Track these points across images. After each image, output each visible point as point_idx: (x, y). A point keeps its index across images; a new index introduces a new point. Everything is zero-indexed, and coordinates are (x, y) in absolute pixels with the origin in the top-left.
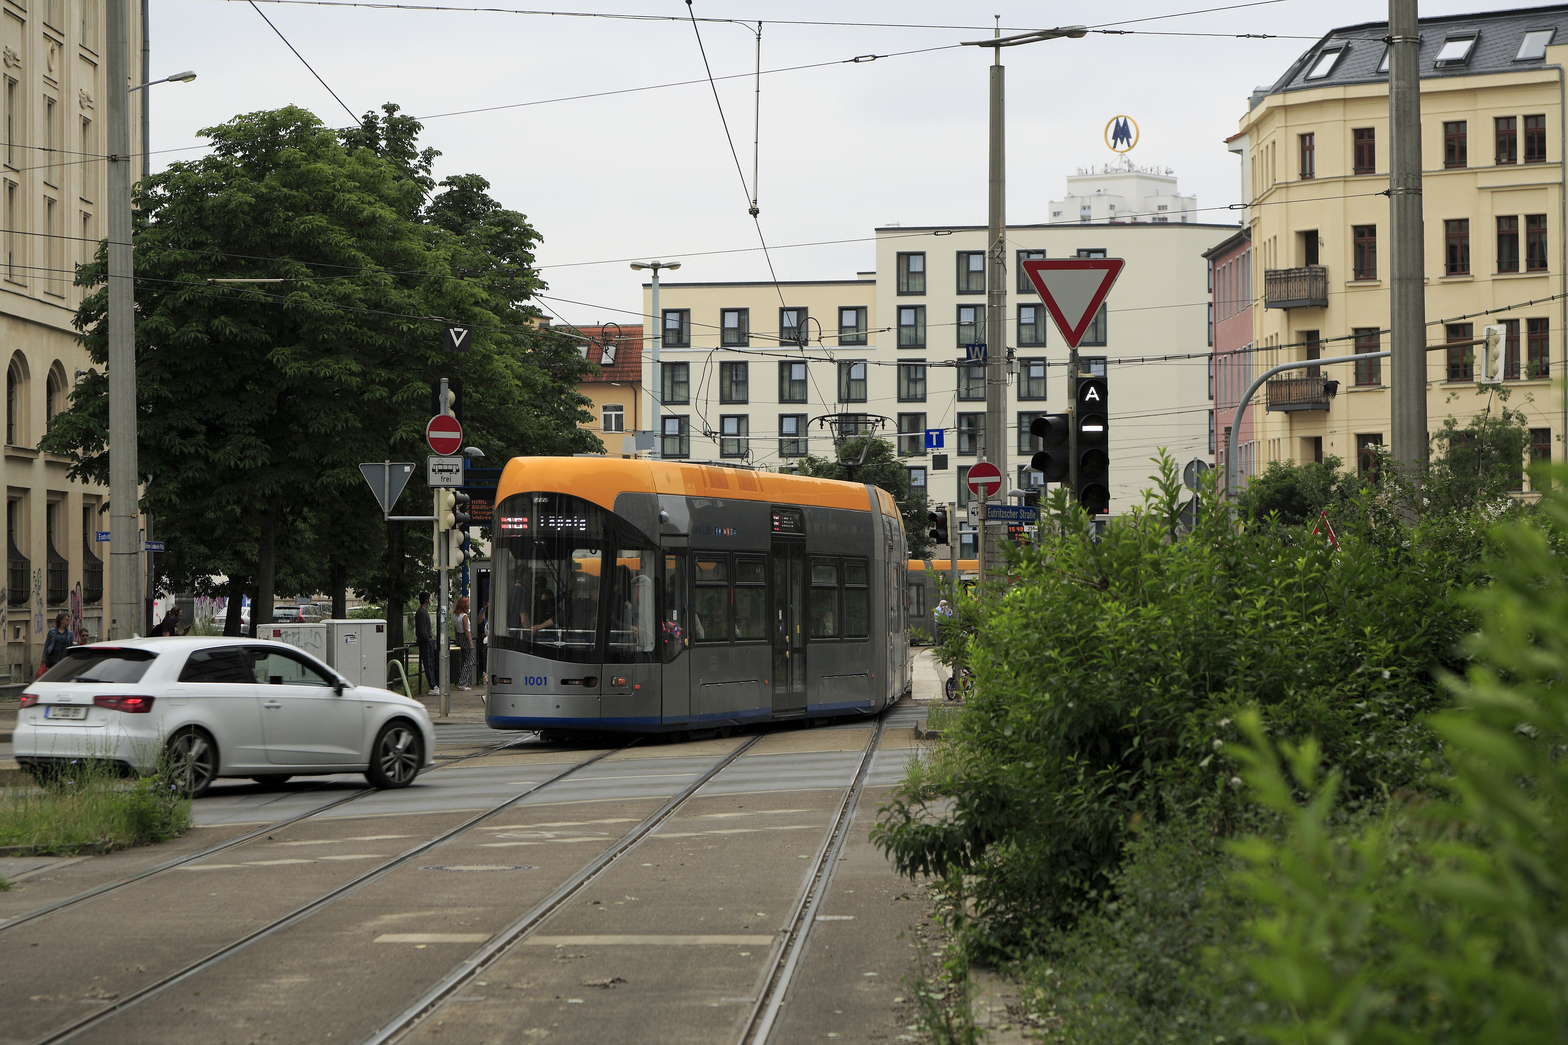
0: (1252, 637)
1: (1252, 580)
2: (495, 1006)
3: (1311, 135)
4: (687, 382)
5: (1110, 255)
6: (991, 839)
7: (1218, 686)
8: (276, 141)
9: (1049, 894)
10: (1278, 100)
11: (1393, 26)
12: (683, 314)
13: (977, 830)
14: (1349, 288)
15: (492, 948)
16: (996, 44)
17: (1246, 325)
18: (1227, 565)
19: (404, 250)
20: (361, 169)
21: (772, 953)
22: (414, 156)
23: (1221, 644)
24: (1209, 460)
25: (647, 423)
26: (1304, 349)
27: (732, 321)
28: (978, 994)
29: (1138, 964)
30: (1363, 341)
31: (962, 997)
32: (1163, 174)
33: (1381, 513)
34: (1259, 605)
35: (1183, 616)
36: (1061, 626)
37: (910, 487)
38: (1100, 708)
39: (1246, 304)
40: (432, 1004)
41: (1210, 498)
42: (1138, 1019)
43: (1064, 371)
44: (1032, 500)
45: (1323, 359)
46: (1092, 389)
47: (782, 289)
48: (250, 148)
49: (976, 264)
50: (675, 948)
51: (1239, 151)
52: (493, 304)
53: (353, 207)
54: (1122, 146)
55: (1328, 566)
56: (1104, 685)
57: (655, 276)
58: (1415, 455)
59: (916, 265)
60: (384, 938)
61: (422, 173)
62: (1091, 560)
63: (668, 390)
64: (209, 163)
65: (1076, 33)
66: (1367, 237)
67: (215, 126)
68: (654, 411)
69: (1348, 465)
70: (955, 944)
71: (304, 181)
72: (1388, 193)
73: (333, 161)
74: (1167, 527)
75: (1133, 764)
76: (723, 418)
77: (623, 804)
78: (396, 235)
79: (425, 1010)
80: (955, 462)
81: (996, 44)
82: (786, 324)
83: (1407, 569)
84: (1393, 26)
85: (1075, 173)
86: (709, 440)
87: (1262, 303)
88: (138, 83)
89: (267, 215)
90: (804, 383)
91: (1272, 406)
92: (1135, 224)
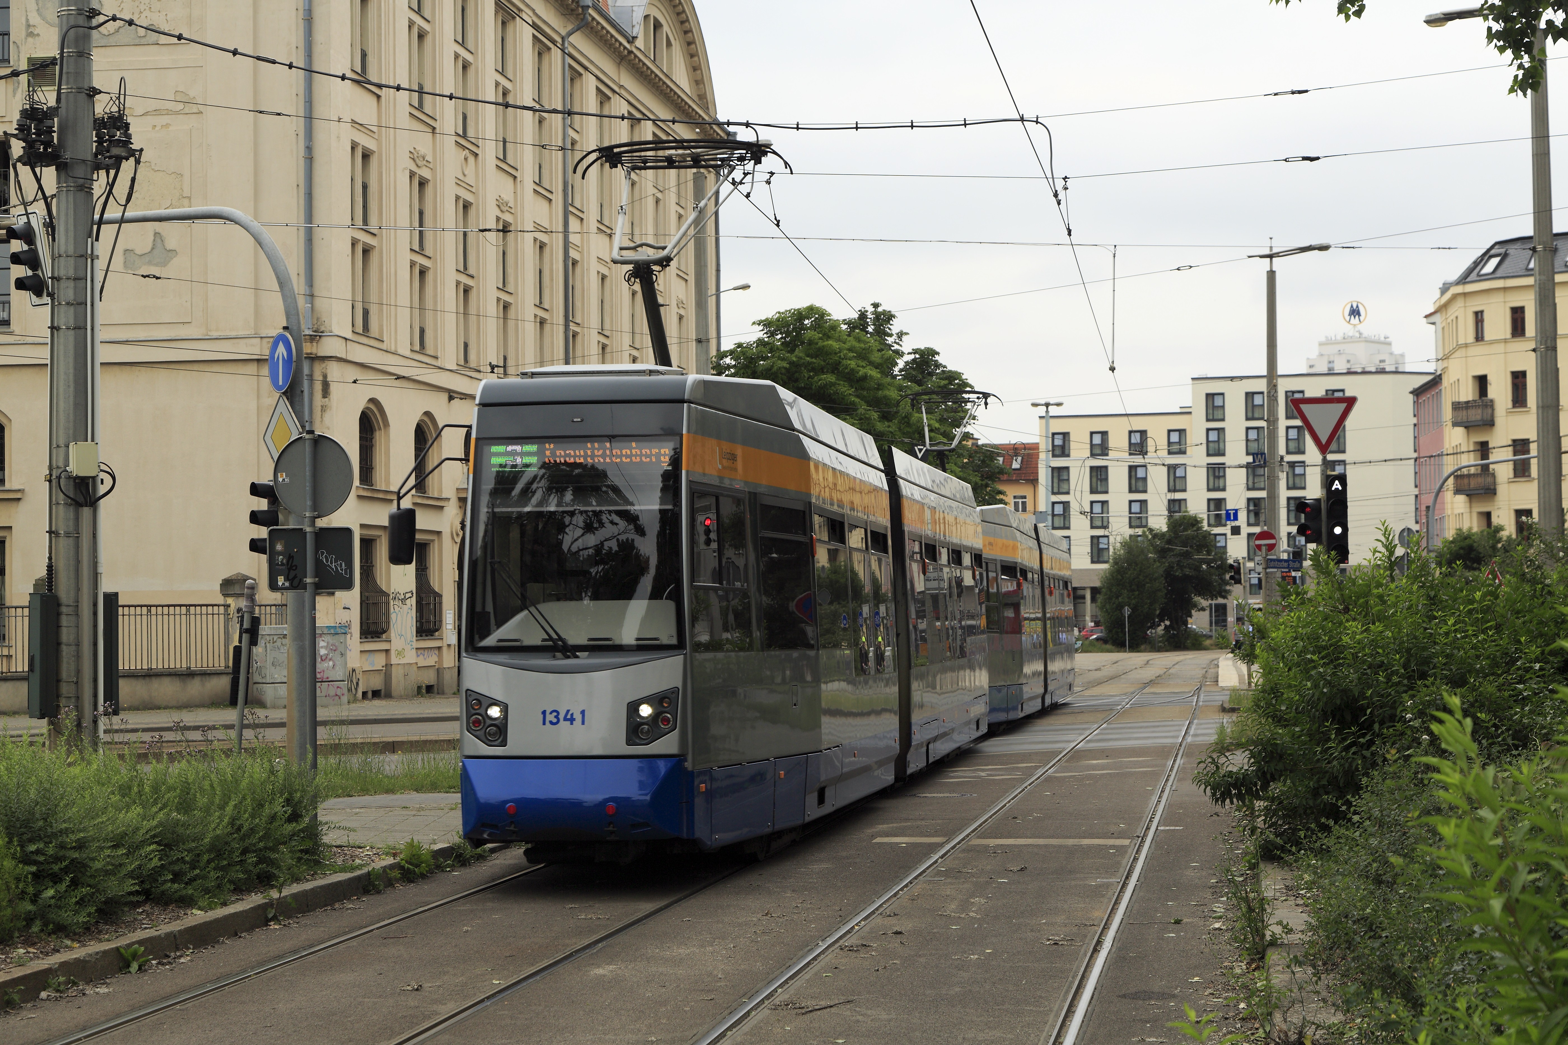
0: (1445, 644)
1: (1446, 607)
2: (951, 884)
3: (1482, 312)
4: (1068, 480)
5: (1348, 394)
6: (1273, 779)
7: (1423, 676)
8: (803, 327)
9: (1312, 813)
10: (1459, 289)
11: (1536, 239)
12: (1065, 435)
13: (1264, 773)
14: (1509, 413)
15: (948, 847)
16: (1271, 257)
17: (1439, 438)
18: (1429, 598)
19: (885, 397)
20: (857, 345)
21: (1130, 850)
22: (891, 335)
23: (1425, 649)
24: (1415, 527)
25: (1042, 506)
26: (1479, 454)
27: (1097, 440)
28: (1266, 877)
29: (1372, 858)
30: (1518, 448)
31: (1256, 878)
32: (1382, 339)
33: (1531, 561)
34: (1450, 623)
35: (1400, 632)
36: (1318, 638)
37: (1216, 547)
38: (1345, 691)
39: (1439, 424)
40: (911, 882)
41: (1416, 553)
42: (1372, 893)
43: (1318, 470)
44: (1298, 555)
45: (1492, 459)
46: (1337, 482)
47: (1131, 418)
48: (785, 332)
49: (1258, 400)
50: (1066, 847)
51: (1433, 323)
52: (942, 430)
53: (852, 370)
54: (1355, 321)
55: (1497, 597)
56: (1347, 676)
57: (1047, 412)
58: (1554, 524)
59: (1218, 401)
60: (878, 840)
61: (896, 347)
62: (1337, 595)
63: (1056, 485)
64: (760, 342)
65: (1324, 248)
66: (1520, 379)
67: (763, 318)
68: (1047, 498)
69: (1509, 530)
70: (1250, 845)
71: (820, 353)
72: (1534, 350)
73: (838, 340)
74: (1388, 573)
75: (1367, 727)
76: (1092, 503)
77: (1030, 754)
78: (880, 387)
79: (906, 886)
80: (1245, 530)
81: (1271, 257)
82: (1133, 441)
83: (1549, 598)
84: (1536, 239)
85: (1323, 339)
86: (1083, 517)
87: (1450, 424)
88: (714, 292)
89: (797, 375)
90: (1145, 479)
91: (1458, 491)
92: (1364, 373)
